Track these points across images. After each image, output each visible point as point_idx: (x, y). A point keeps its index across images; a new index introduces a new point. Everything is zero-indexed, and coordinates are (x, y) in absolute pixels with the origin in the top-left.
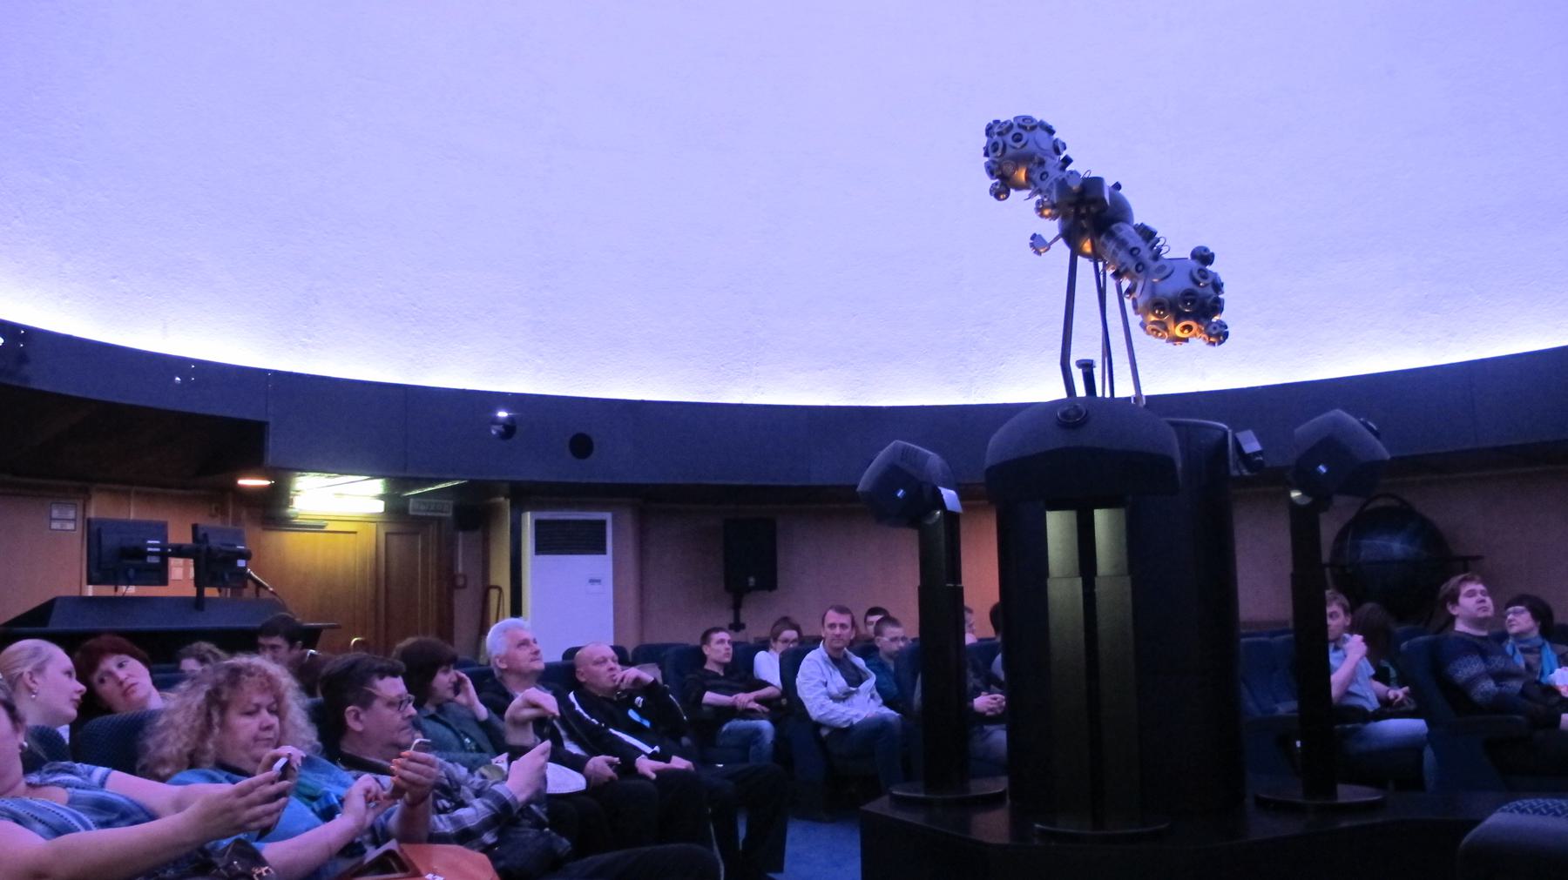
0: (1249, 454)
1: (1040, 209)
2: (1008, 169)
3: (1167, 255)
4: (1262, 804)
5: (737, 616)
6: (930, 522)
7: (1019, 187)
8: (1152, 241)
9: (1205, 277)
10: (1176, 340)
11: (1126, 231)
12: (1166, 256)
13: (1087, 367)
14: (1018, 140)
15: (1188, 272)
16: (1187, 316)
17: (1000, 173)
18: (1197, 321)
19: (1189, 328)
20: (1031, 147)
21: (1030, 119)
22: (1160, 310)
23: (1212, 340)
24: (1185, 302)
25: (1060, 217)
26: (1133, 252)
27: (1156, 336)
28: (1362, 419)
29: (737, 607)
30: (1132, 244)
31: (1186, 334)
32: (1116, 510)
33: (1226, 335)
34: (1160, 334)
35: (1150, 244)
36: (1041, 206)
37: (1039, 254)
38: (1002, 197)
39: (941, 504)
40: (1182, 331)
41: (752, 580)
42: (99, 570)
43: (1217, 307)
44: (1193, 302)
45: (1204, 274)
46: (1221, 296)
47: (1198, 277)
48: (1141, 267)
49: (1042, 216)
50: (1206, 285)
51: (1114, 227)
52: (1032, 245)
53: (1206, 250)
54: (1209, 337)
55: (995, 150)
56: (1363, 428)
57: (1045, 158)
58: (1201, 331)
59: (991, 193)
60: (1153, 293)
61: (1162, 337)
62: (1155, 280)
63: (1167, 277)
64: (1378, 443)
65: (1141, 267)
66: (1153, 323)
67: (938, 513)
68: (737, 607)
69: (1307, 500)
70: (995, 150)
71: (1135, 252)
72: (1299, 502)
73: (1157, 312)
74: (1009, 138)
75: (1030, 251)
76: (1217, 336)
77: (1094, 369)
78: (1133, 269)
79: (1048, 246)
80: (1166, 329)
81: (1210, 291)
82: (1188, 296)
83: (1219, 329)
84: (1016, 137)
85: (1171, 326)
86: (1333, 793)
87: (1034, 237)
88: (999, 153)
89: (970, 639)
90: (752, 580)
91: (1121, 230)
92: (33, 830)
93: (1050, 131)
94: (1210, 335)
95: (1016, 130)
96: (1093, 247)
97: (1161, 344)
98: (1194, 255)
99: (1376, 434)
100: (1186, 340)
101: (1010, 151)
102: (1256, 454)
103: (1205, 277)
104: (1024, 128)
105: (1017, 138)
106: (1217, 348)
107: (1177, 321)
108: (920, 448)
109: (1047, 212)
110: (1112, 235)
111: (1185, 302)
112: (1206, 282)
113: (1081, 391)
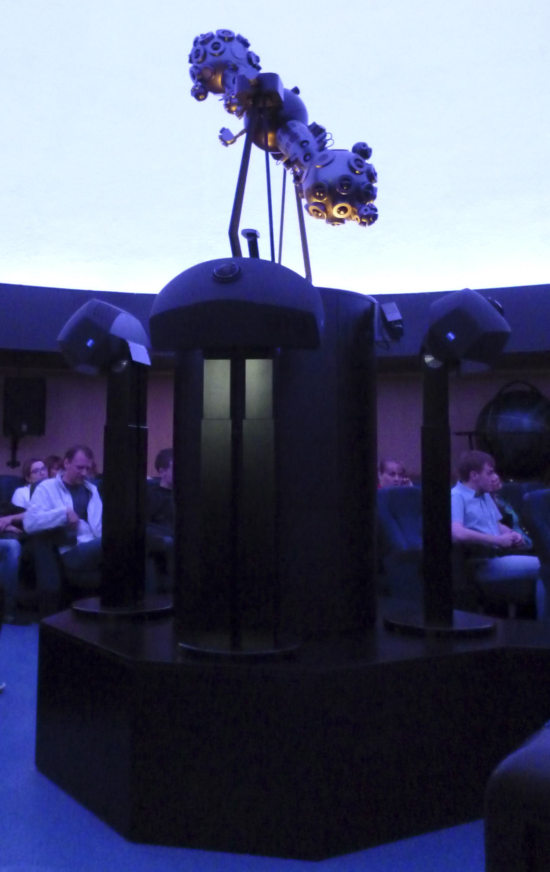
0: (391, 322)
1: (228, 107)
2: (208, 73)
3: (330, 146)
4: (390, 627)
5: (14, 455)
6: (117, 370)
7: (216, 91)
8: (321, 136)
9: (360, 166)
10: (333, 220)
11: (298, 127)
12: (329, 148)
13: (252, 236)
14: (216, 49)
15: (345, 163)
16: (343, 199)
17: (200, 77)
18: (352, 205)
19: (344, 209)
20: (227, 56)
21: (229, 32)
22: (320, 193)
23: (364, 221)
24: (342, 186)
25: (245, 114)
26: (303, 144)
27: (317, 215)
28: (490, 298)
29: (14, 448)
30: (302, 137)
31: (342, 215)
32: (265, 360)
33: (375, 217)
34: (320, 214)
35: (318, 139)
36: (228, 102)
37: (226, 144)
38: (201, 97)
39: (128, 356)
40: (339, 212)
41: (24, 427)
42: (166, 467)
43: (371, 194)
44: (349, 186)
45: (361, 165)
46: (375, 185)
47: (355, 167)
48: (308, 157)
49: (230, 111)
50: (361, 173)
51: (290, 123)
52: (221, 138)
53: (364, 145)
54: (361, 218)
55: (197, 57)
56: (488, 304)
57: (238, 65)
58: (355, 213)
59: (192, 94)
60: (316, 177)
61: (322, 217)
62: (318, 167)
63: (326, 165)
64: (503, 319)
65: (308, 157)
66: (316, 204)
67: (125, 363)
68: (14, 448)
69: (438, 365)
70: (197, 57)
71: (305, 144)
72: (431, 365)
73: (317, 194)
74: (209, 47)
75: (219, 143)
76: (367, 217)
77: (259, 240)
78: (301, 159)
79: (234, 139)
80: (325, 210)
81: (364, 178)
82: (345, 181)
83: (369, 211)
84: (215, 46)
85: (329, 209)
86: (449, 618)
87: (223, 130)
88: (200, 59)
89: (149, 478)
90: (24, 427)
91: (295, 126)
92: (494, 500)
93: (246, 44)
94: (361, 217)
95: (216, 40)
96: (275, 140)
97: (322, 222)
98: (355, 149)
99: (501, 311)
100: (342, 221)
101: (210, 59)
102: (396, 322)
103: (360, 166)
104: (223, 38)
105: (216, 46)
106: (368, 228)
107: (334, 204)
108: (111, 305)
109: (234, 108)
110: (287, 131)
111: (342, 186)
112: (362, 170)
113: (245, 253)
